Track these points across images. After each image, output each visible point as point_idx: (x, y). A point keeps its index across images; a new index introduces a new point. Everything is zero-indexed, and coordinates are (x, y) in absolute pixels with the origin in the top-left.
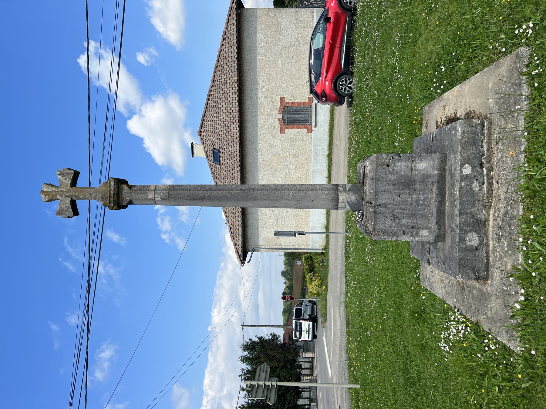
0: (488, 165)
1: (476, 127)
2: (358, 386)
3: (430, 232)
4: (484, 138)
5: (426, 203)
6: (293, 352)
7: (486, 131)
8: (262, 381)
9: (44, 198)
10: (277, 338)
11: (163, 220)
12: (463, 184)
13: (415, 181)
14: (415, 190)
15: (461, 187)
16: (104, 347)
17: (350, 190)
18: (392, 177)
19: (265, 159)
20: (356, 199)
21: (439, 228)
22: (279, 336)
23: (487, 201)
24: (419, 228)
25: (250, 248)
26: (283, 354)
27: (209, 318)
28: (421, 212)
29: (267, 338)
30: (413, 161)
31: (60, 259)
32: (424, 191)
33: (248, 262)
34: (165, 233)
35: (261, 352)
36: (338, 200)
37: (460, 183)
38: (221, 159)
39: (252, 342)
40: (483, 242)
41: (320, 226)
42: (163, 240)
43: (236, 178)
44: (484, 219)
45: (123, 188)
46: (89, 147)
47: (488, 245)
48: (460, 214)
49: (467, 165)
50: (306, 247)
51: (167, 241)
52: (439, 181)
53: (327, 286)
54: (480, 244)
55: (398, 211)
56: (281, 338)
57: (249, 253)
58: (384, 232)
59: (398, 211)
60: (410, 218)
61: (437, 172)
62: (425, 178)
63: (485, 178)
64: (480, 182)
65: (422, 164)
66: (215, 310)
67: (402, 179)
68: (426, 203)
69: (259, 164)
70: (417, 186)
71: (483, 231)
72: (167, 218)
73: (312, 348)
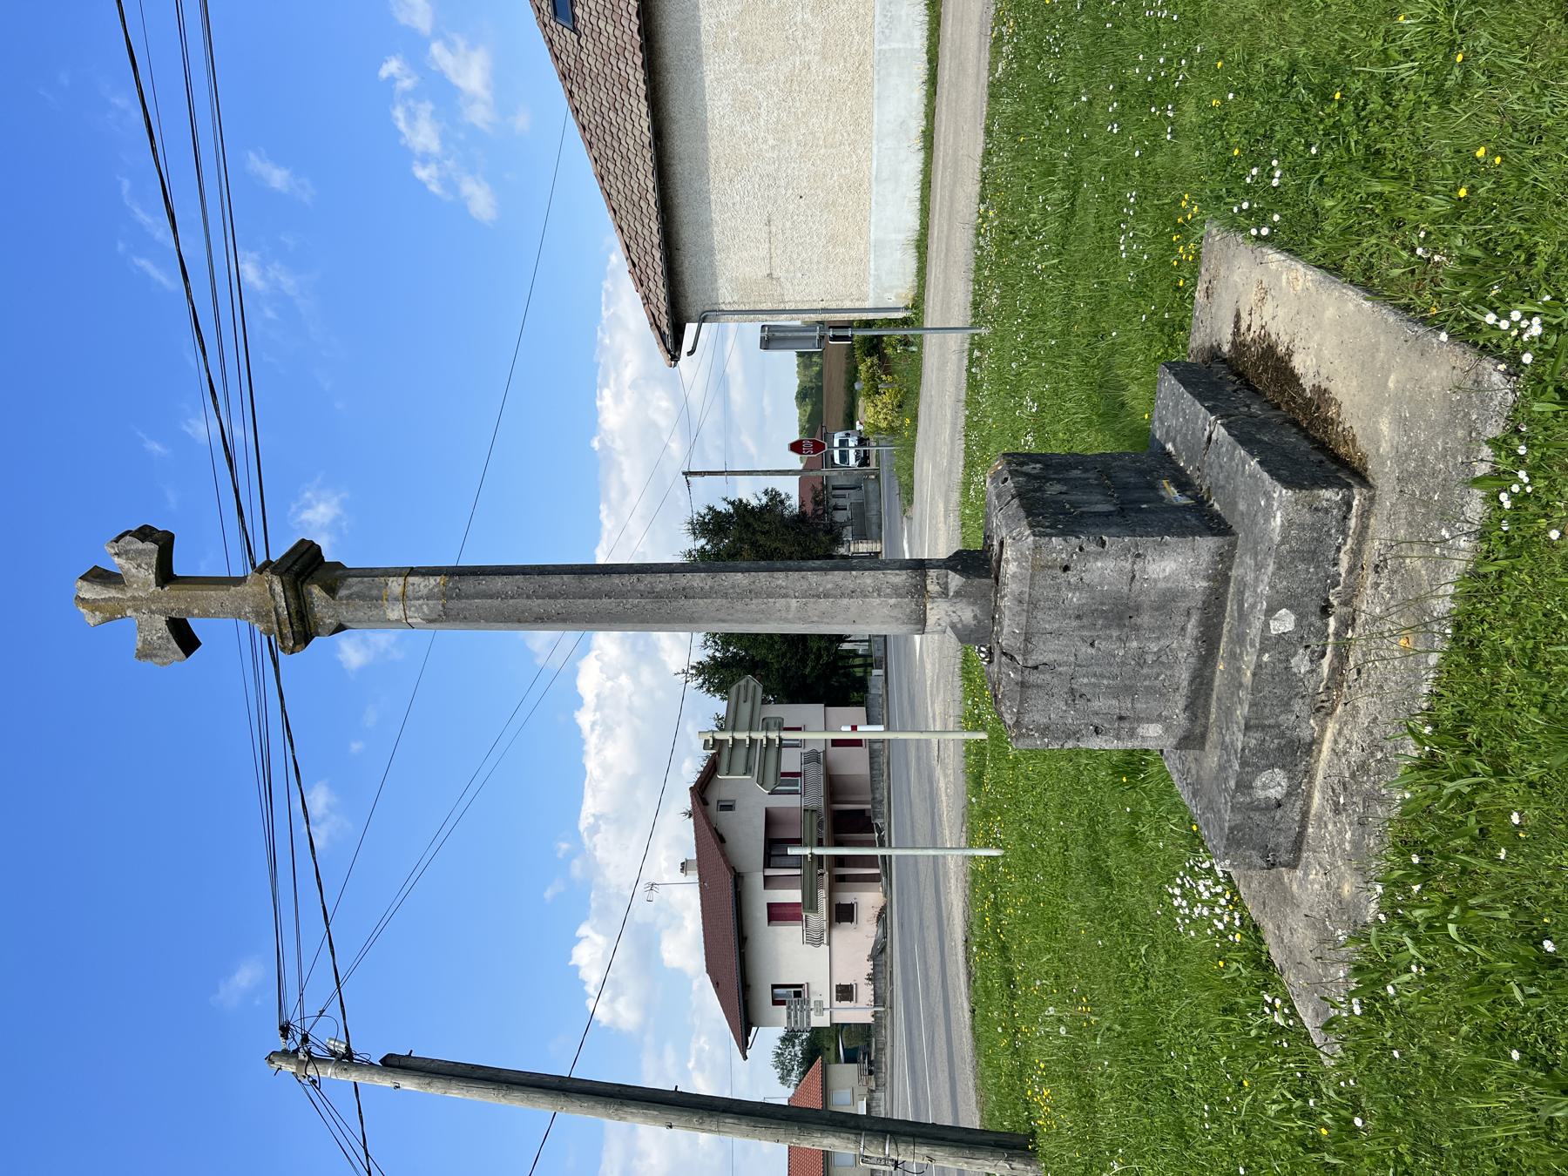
0: (1345, 609)
1: (1327, 511)
2: (983, 736)
3: (1167, 730)
4: (1345, 540)
5: (1164, 659)
6: (825, 539)
7: (1353, 523)
8: (743, 730)
9: (92, 619)
10: (782, 502)
11: (412, 116)
12: (1266, 658)
13: (1138, 609)
14: (1137, 628)
15: (1259, 666)
16: (308, 495)
17: (958, 594)
18: (1075, 598)
19: (723, 19)
20: (975, 617)
21: (1193, 718)
22: (788, 497)
23: (1323, 697)
24: (1140, 720)
25: (694, 310)
26: (800, 544)
27: (590, 419)
28: (1147, 683)
29: (754, 503)
30: (1138, 556)
31: (121, 247)
32: (1161, 631)
33: (690, 353)
34: (425, 159)
35: (741, 540)
36: (925, 620)
37: (1259, 656)
38: (578, 11)
39: (716, 514)
40: (1297, 790)
41: (901, 237)
42: (422, 185)
43: (632, 87)
44: (1308, 739)
45: (310, 593)
46: (154, 150)
47: (1310, 796)
48: (1248, 728)
49: (1284, 611)
50: (858, 305)
51: (434, 188)
52: (1206, 606)
53: (915, 418)
54: (1288, 795)
55: (1085, 680)
56: (794, 502)
57: (691, 329)
58: (1045, 730)
59: (1085, 680)
60: (1117, 698)
61: (1205, 584)
62: (1167, 601)
63: (1331, 640)
64: (1313, 652)
65: (1163, 564)
66: (607, 393)
67: (1102, 604)
68: (1164, 659)
69: (703, 38)
70: (1145, 619)
71: (1302, 767)
72: (426, 108)
73: (874, 528)
